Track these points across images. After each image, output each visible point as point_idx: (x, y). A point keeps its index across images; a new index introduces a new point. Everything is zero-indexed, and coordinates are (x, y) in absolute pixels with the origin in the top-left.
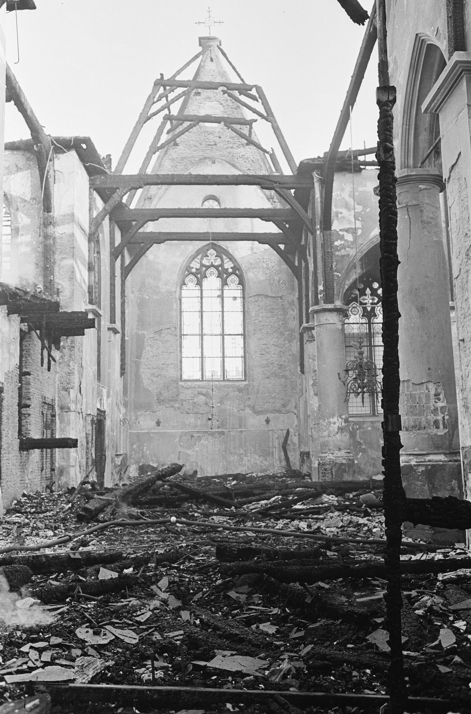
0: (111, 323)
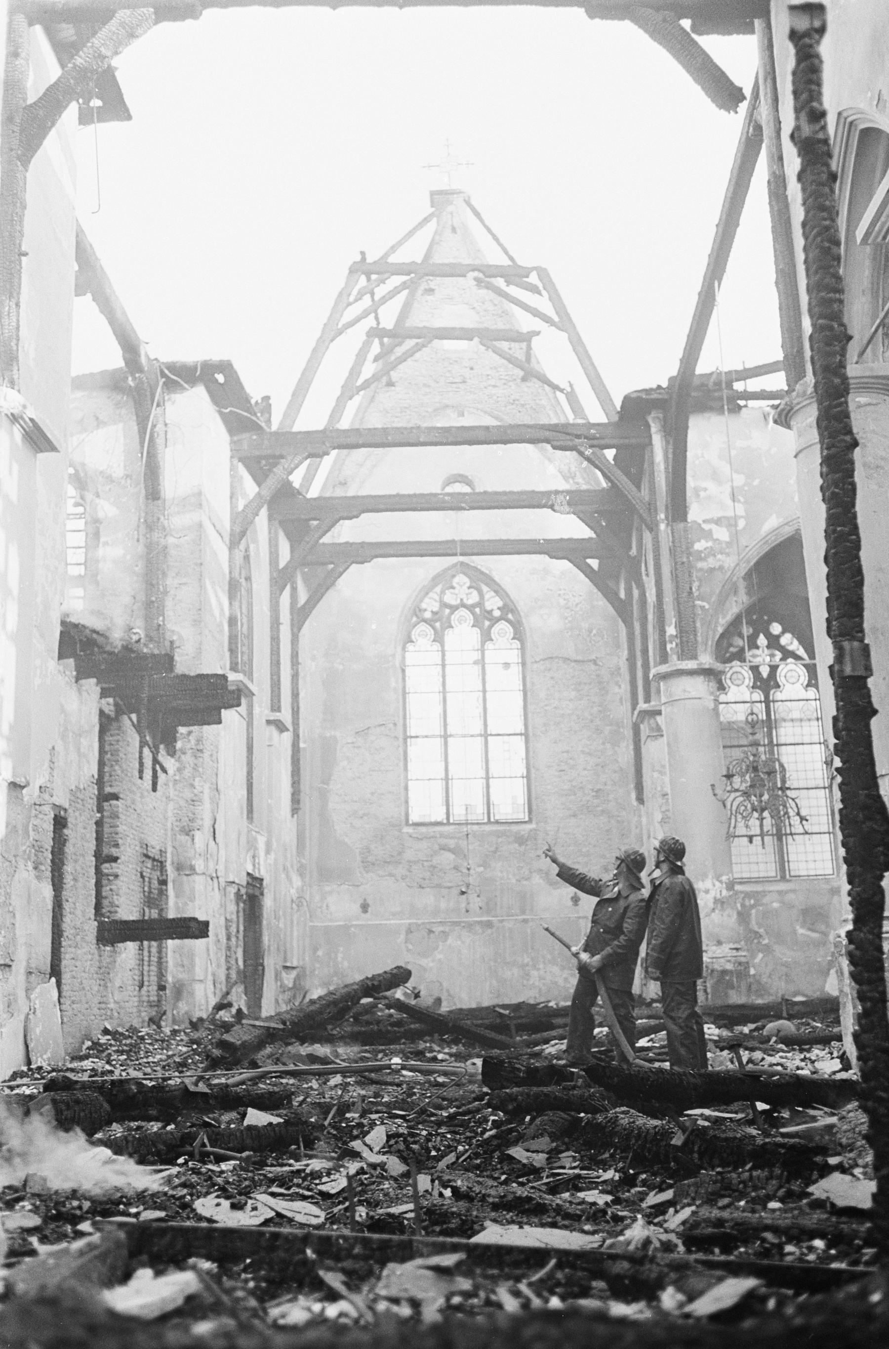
0: (273, 710)
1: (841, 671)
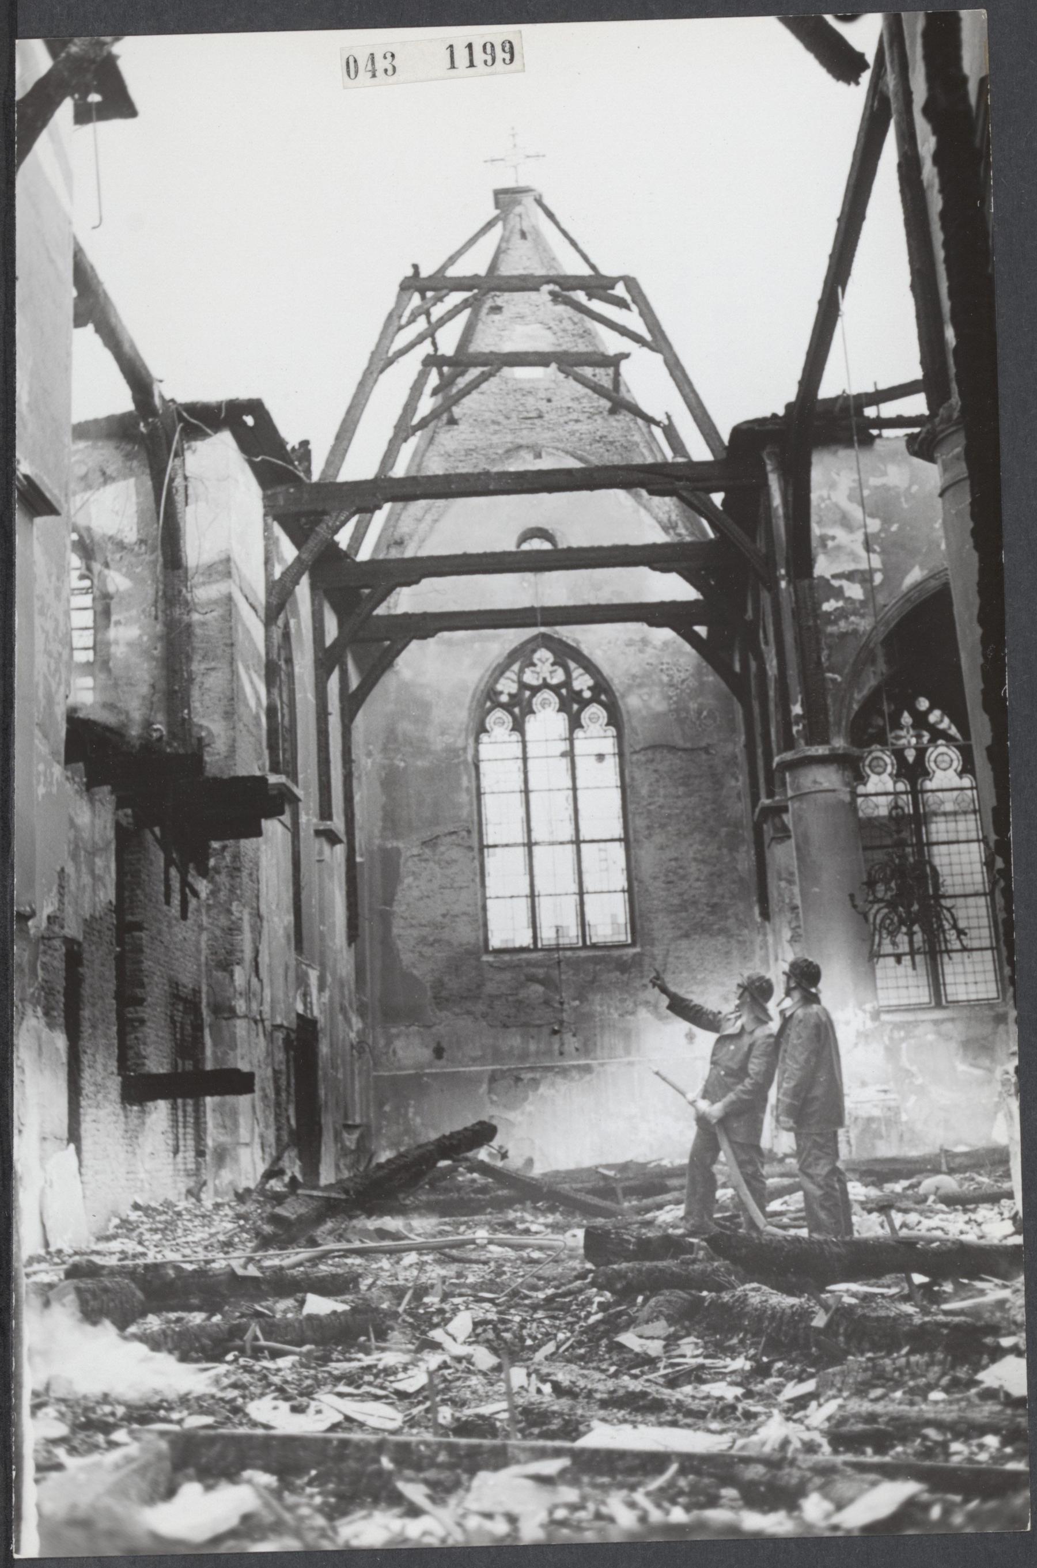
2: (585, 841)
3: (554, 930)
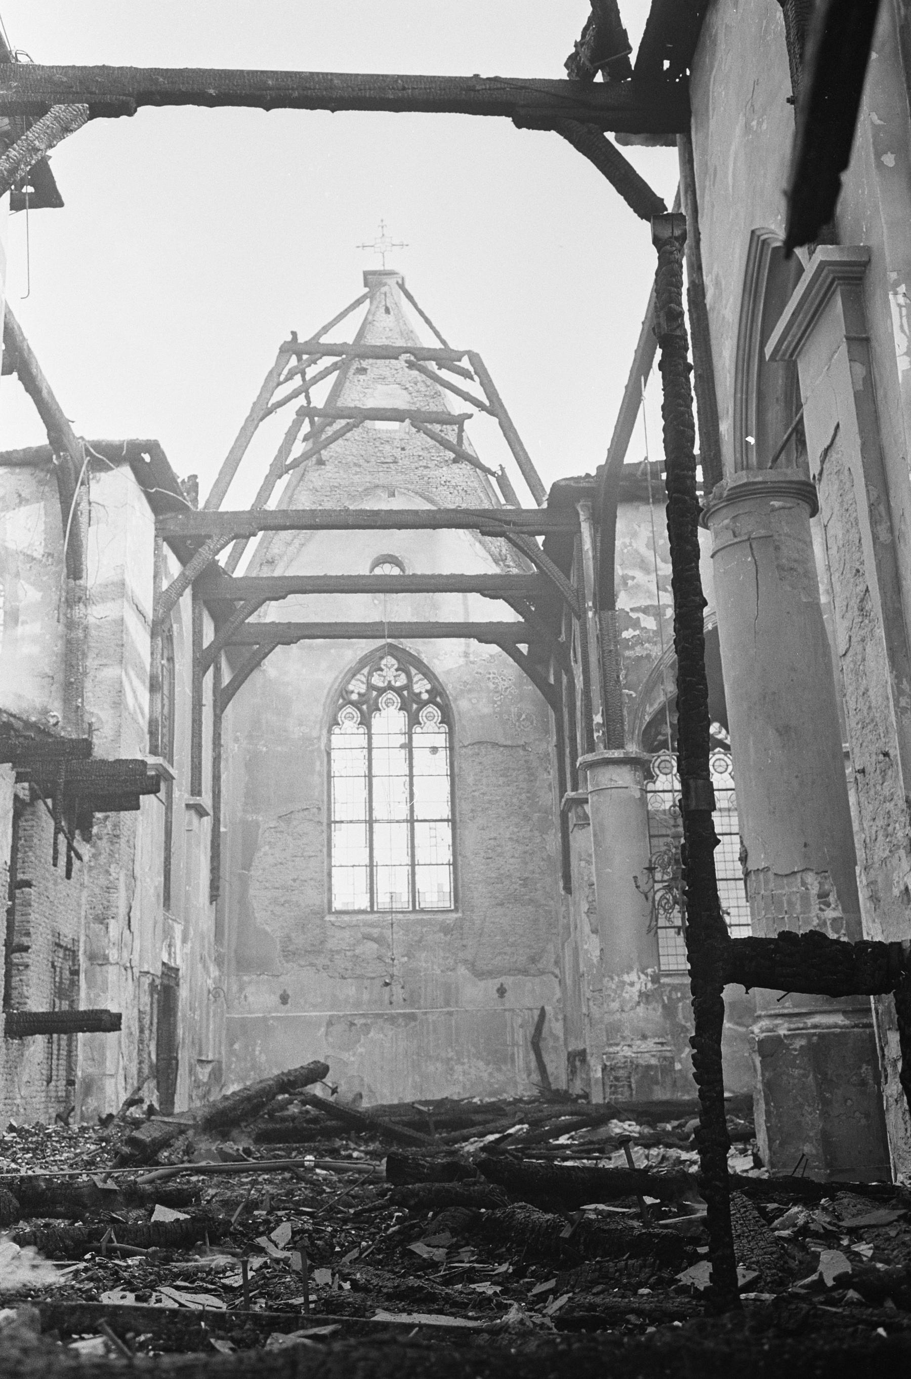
1: (688, 806)
2: (418, 821)
3: (389, 895)
